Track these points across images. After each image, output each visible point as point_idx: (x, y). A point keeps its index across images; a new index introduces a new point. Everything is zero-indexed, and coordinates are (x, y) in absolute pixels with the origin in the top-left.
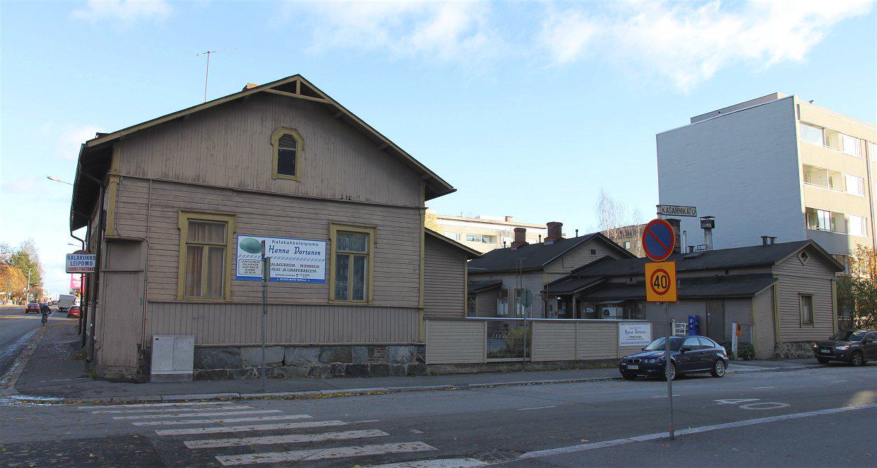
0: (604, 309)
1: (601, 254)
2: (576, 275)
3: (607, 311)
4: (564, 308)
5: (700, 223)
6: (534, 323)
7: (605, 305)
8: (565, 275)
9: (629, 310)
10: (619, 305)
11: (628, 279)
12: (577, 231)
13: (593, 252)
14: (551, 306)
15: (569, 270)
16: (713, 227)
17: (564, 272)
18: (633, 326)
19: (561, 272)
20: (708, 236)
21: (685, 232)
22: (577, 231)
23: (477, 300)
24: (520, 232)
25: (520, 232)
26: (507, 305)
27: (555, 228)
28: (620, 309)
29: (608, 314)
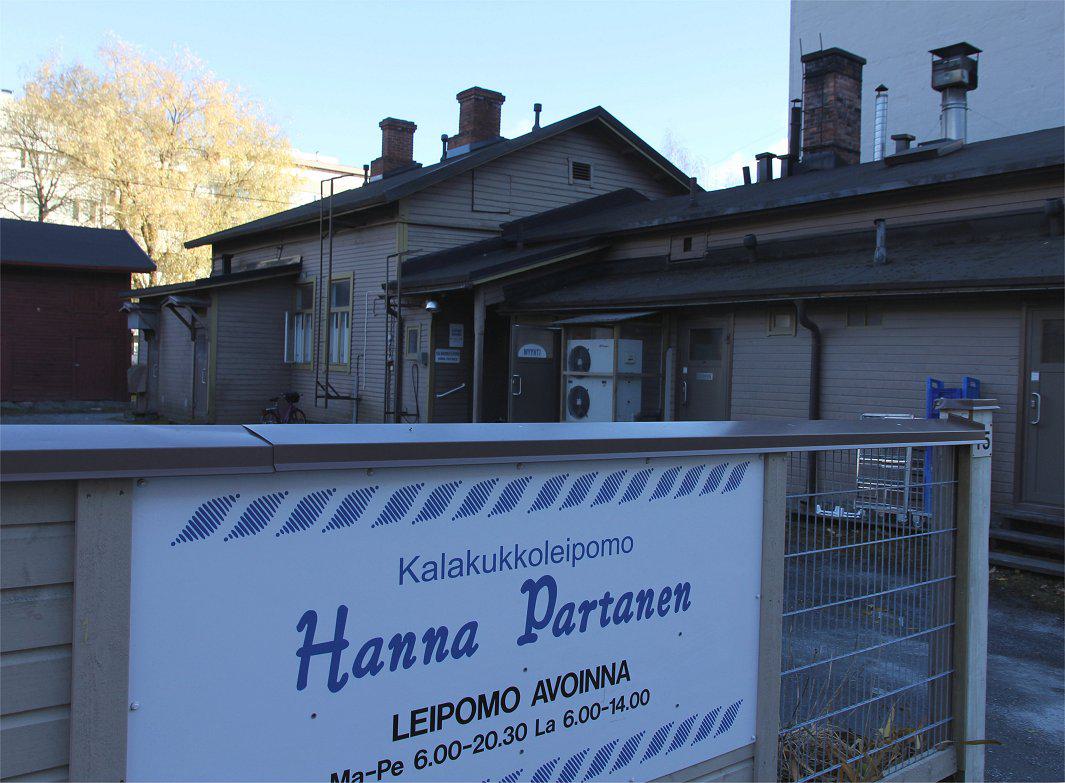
0: (574, 344)
1: (607, 179)
2: (515, 236)
3: (582, 353)
4: (456, 341)
5: (930, 66)
6: (374, 390)
7: (586, 331)
8: (477, 238)
9: (670, 353)
10: (626, 330)
11: (679, 243)
12: (538, 108)
13: (581, 172)
14: (414, 334)
15: (494, 222)
16: (973, 84)
17: (477, 224)
18: (486, 532)
19: (463, 223)
20: (953, 115)
21: (882, 89)
22: (538, 108)
23: (213, 313)
24: (398, 133)
25: (398, 133)
26: (347, 332)
27: (481, 106)
28: (634, 348)
29: (587, 366)
